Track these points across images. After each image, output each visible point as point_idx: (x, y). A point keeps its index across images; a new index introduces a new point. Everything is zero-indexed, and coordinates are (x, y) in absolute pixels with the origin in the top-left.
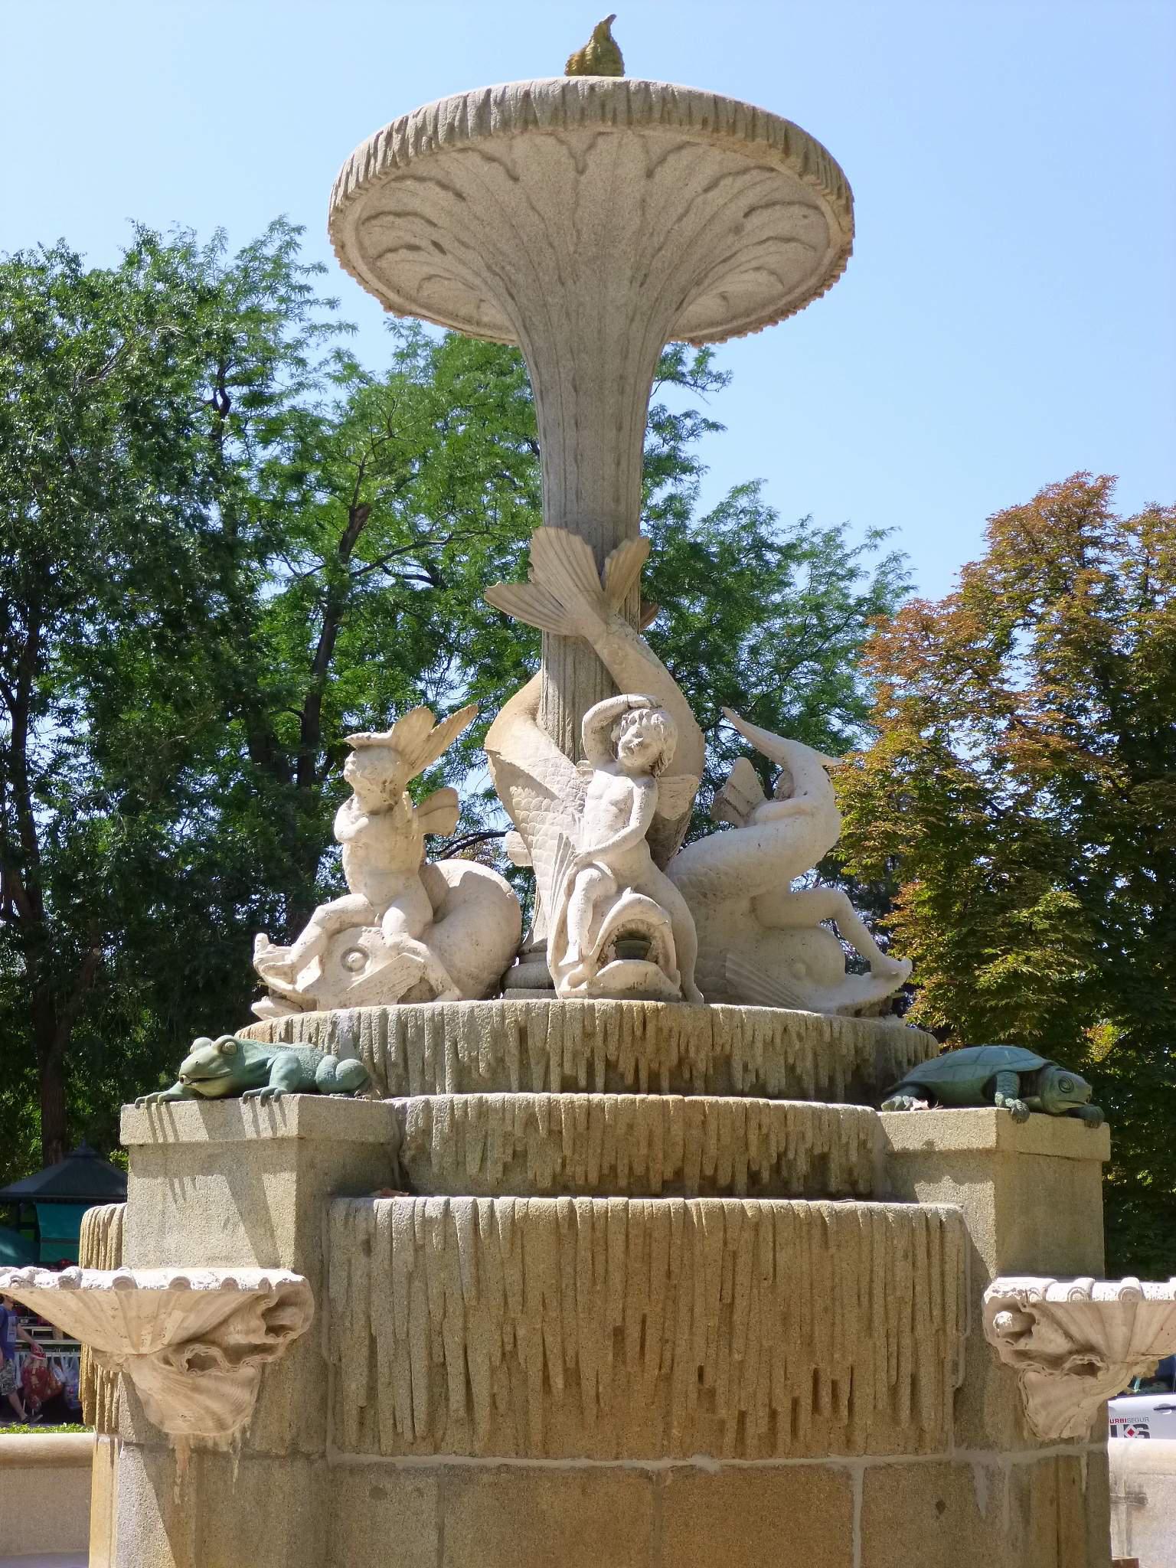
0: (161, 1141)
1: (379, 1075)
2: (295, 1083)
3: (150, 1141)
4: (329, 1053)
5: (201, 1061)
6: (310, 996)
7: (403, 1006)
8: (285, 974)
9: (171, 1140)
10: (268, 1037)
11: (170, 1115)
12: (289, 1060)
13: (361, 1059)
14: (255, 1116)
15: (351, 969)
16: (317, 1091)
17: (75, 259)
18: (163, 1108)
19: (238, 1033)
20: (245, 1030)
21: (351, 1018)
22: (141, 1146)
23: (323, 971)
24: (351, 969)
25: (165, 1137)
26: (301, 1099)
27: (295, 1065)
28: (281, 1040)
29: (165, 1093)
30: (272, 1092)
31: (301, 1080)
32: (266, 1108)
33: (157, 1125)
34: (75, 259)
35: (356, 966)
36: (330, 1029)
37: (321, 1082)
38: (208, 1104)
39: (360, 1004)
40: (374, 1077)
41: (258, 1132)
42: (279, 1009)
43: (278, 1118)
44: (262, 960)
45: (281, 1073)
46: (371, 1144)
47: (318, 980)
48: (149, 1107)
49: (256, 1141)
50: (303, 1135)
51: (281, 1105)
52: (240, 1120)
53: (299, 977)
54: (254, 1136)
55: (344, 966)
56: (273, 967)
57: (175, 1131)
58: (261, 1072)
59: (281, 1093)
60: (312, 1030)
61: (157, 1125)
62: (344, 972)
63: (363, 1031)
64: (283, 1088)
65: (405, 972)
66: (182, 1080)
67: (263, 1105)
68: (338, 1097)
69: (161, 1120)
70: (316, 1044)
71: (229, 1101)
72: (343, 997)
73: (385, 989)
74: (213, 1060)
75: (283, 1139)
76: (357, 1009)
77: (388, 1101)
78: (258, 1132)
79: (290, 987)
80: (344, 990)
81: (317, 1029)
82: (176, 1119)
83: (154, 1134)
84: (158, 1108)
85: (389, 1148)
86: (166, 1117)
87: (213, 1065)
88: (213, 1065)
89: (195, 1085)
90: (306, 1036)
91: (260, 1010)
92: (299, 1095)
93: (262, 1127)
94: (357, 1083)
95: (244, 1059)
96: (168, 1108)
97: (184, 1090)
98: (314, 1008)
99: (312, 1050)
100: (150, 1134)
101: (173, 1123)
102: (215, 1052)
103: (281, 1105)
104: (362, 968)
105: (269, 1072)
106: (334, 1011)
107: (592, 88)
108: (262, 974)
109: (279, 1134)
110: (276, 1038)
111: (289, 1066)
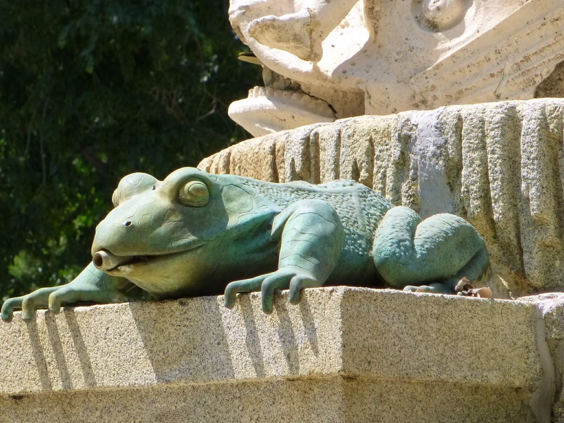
0: (58, 387)
1: (505, 247)
2: (333, 263)
3: (36, 388)
4: (397, 201)
5: (136, 221)
6: (348, 85)
7: (550, 102)
8: (297, 39)
9: (79, 385)
10: (267, 171)
11: (76, 332)
12: (317, 217)
13: (465, 214)
14: (252, 333)
15: (434, 27)
16: (378, 282)
17: (369, 58)
18: (61, 320)
19: (205, 163)
20: (218, 158)
21: (440, 128)
22: (17, 398)
23: (375, 31)
24: (434, 27)
25: (66, 378)
26: (347, 296)
27: (330, 227)
28: (295, 176)
29: (62, 289)
30: (285, 282)
31: (343, 257)
32: (275, 316)
33: (49, 355)
34: (369, 58)
35: (444, 19)
36: (396, 152)
37: (384, 261)
38: (152, 308)
39: (450, 100)
40: (493, 249)
41: (259, 366)
42: (286, 113)
43: (300, 335)
44: (246, 10)
45: (301, 245)
46: (498, 391)
47: (364, 51)
48: (30, 319)
49: (256, 385)
50: (354, 371)
51: (305, 311)
52: (221, 340)
53: (326, 44)
54: (251, 374)
55: (419, 20)
56: (271, 25)
57: (87, 366)
58: (260, 241)
59: (303, 285)
60: (360, 154)
61: (49, 355)
62: (420, 32)
63: (468, 156)
64: (309, 276)
65: (550, 29)
66: (99, 262)
67: (267, 310)
68: (420, 292)
69: (57, 345)
70: (368, 183)
71: (195, 303)
72: (418, 86)
73: (508, 66)
74: (160, 219)
75: (311, 380)
76: (453, 109)
77: (526, 300)
78: (259, 366)
79: (306, 66)
80: (420, 69)
81: (370, 152)
82: (88, 341)
83: (44, 372)
84: (49, 319)
85: (533, 398)
86: (66, 337)
87: (163, 229)
88: (163, 229)
89: (126, 271)
90: (346, 168)
91: (247, 114)
92: (341, 289)
93: (266, 354)
94: (458, 263)
95: (223, 215)
96: (71, 320)
97: (102, 282)
98: (359, 110)
99: (363, 196)
100: (35, 373)
101: (81, 349)
102: (165, 203)
103: (305, 311)
104: (458, 22)
105: (277, 241)
106: (405, 115)
107: (452, 299)
108: (248, 40)
109: (304, 370)
110: (285, 171)
111: (319, 228)
